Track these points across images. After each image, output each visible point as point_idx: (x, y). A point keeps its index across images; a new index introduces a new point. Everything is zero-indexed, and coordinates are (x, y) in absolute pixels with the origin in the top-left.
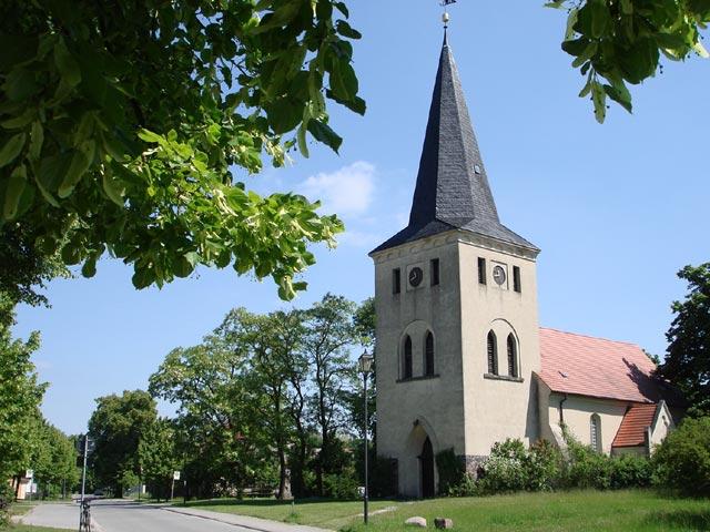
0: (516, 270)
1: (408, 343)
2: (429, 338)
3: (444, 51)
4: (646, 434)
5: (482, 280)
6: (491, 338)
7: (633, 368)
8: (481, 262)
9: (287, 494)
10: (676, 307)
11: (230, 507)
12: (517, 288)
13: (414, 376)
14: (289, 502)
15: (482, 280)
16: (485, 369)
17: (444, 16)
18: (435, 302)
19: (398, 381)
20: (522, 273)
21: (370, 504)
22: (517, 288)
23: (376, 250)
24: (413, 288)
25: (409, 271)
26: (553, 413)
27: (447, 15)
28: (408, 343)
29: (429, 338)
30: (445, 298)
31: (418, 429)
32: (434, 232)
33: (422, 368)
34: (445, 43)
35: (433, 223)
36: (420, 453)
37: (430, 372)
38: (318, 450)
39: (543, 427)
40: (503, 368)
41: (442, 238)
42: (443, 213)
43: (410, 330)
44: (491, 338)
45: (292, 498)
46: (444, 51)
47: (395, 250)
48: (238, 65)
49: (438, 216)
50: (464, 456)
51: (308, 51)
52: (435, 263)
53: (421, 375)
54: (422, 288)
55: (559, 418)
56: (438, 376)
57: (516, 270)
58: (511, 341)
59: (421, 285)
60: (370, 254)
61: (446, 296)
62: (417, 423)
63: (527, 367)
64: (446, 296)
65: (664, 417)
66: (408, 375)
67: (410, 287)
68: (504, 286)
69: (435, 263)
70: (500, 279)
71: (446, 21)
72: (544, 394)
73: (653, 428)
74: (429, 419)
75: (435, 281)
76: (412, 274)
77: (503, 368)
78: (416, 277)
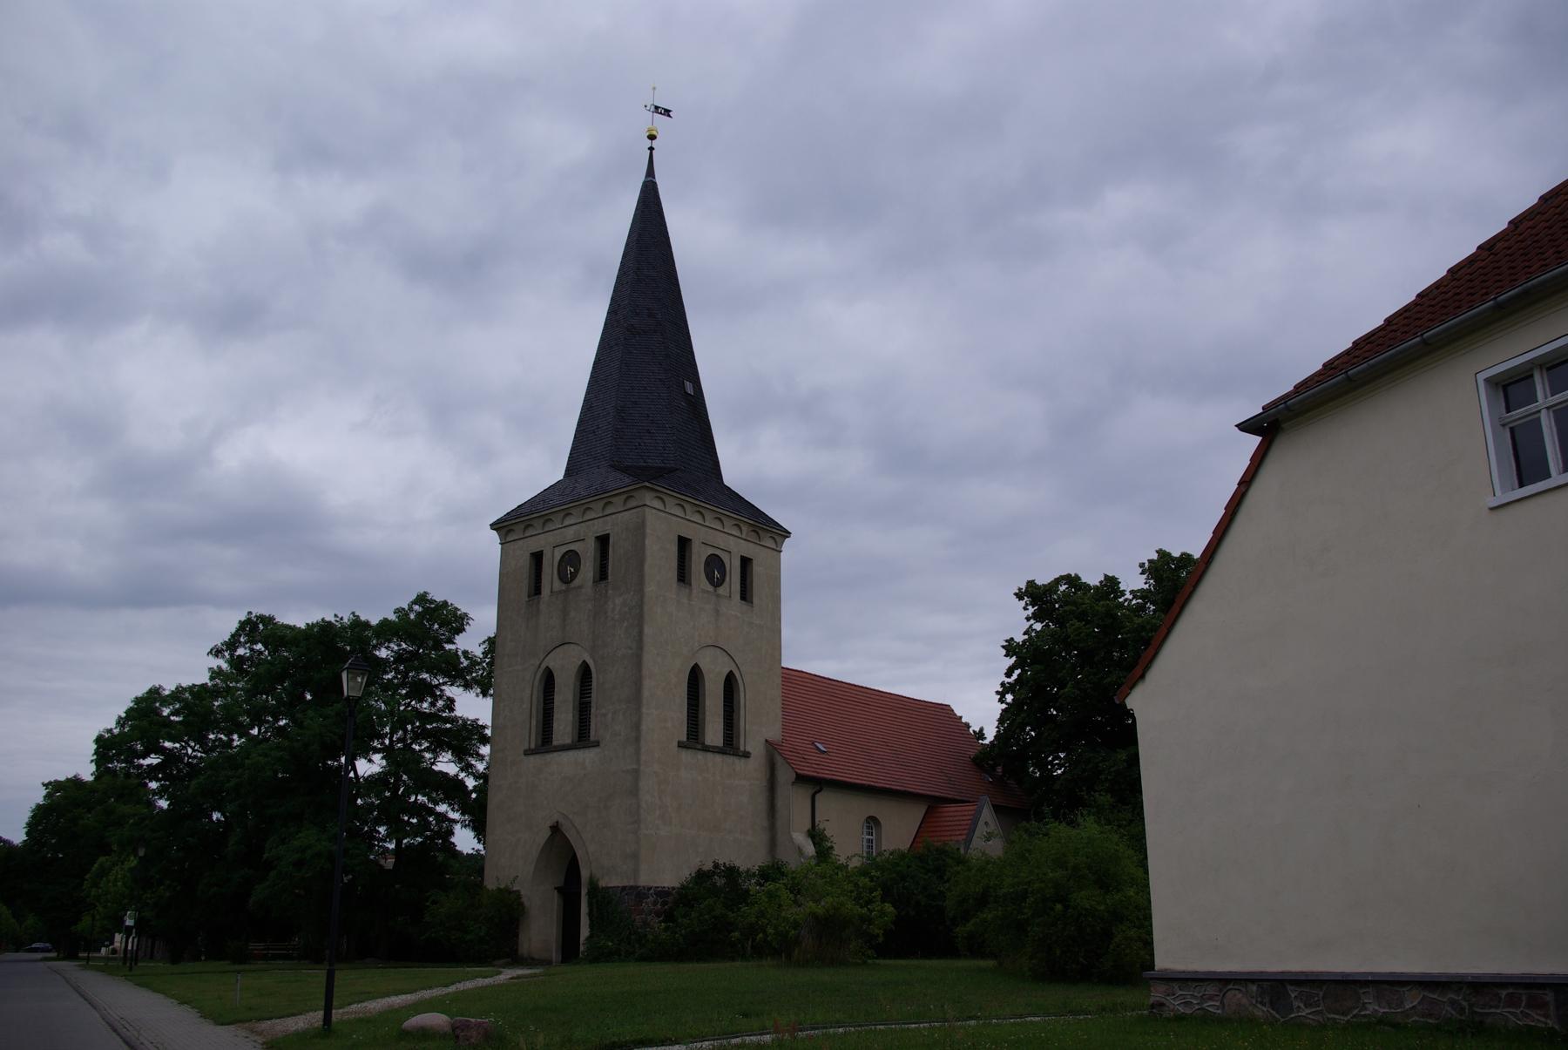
0: (746, 562)
2: (585, 674)
5: (683, 576)
6: (695, 677)
8: (684, 544)
19: (528, 752)
22: (746, 594)
24: (564, 587)
25: (558, 557)
29: (585, 674)
33: (569, 729)
36: (560, 883)
37: (583, 738)
44: (695, 677)
52: (603, 541)
53: (568, 741)
54: (580, 587)
56: (597, 744)
57: (746, 562)
58: (730, 683)
59: (576, 582)
60: (496, 526)
64: (618, 601)
67: (558, 585)
69: (603, 541)
75: (602, 574)
77: (714, 732)
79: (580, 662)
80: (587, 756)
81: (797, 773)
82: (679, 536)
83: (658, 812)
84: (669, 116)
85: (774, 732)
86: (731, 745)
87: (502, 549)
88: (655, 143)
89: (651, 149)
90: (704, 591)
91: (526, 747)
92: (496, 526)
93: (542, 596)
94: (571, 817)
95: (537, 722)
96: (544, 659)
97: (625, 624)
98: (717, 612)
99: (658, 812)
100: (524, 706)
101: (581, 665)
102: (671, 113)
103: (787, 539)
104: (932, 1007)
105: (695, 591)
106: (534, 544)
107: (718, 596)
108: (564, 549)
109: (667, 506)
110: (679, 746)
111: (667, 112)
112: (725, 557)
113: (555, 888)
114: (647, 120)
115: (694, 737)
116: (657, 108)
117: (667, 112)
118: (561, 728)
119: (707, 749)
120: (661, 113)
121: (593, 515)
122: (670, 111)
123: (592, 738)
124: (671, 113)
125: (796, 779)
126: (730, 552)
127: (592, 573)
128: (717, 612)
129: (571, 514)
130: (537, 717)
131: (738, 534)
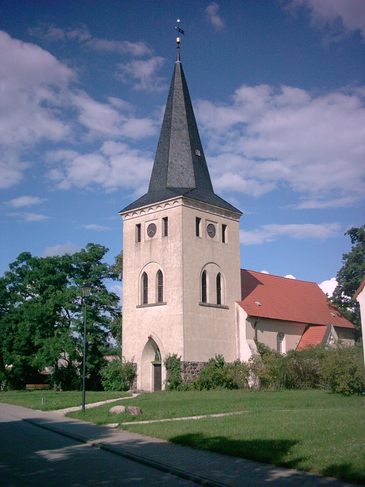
1: (145, 275)
2: (160, 273)
10: (345, 256)
13: (149, 303)
24: (150, 239)
25: (147, 226)
28: (145, 275)
29: (160, 273)
33: (154, 297)
40: (211, 298)
48: (98, 361)
51: (277, 333)
53: (154, 302)
55: (254, 335)
56: (166, 304)
59: (155, 237)
61: (172, 245)
64: (172, 245)
67: (147, 238)
74: (159, 335)
77: (211, 298)
78: (152, 230)
83: (191, 332)
93: (141, 242)
94: (156, 333)
99: (191, 332)
100: (136, 288)
111: (183, 32)
118: (151, 297)
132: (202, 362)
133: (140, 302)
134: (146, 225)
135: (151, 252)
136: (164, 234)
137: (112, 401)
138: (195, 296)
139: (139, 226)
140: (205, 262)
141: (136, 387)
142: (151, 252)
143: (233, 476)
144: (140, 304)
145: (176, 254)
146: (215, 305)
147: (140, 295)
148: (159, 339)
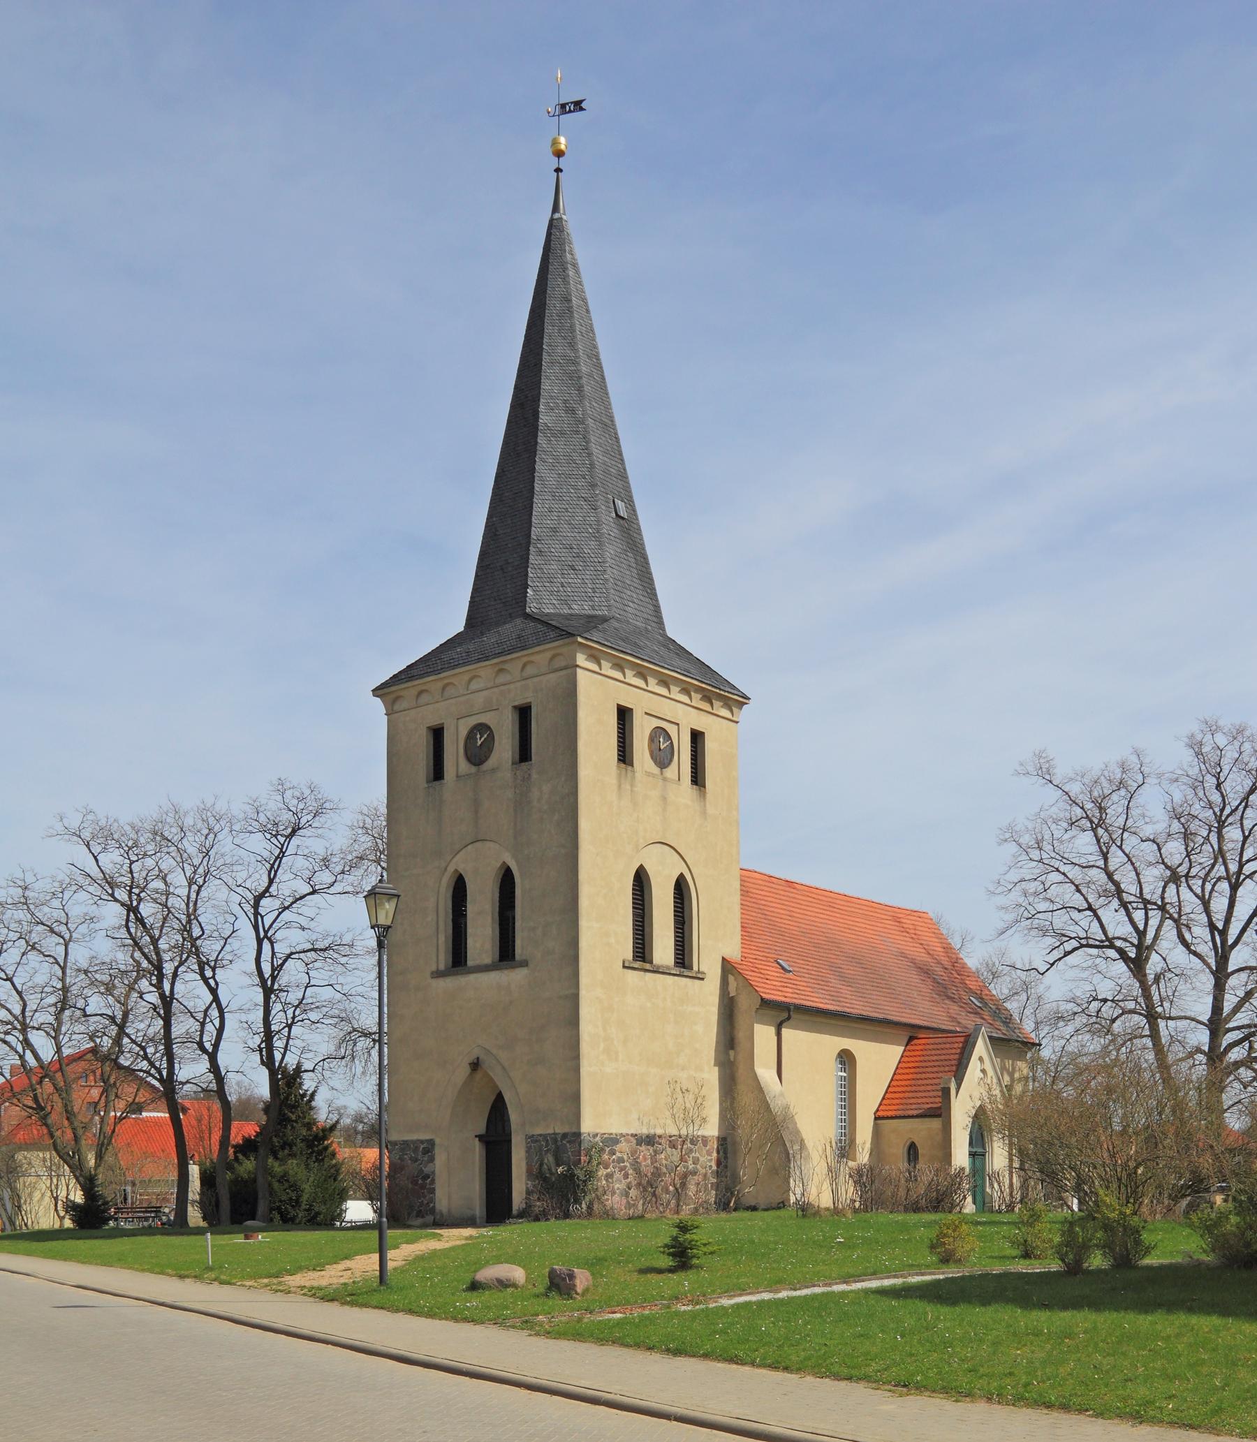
0: (697, 737)
2: (507, 881)
3: (555, 231)
4: (946, 1092)
5: (625, 755)
6: (641, 881)
7: (913, 961)
8: (624, 714)
9: (194, 1216)
11: (807, 1018)
12: (698, 778)
13: (470, 963)
14: (199, 1231)
15: (625, 755)
16: (626, 949)
17: (555, 142)
18: (521, 804)
19: (438, 974)
20: (710, 745)
21: (391, 1233)
22: (698, 778)
23: (396, 679)
24: (473, 769)
25: (464, 732)
26: (763, 1035)
27: (562, 140)
29: (507, 881)
30: (543, 791)
31: (478, 1075)
32: (521, 645)
33: (488, 946)
34: (556, 208)
35: (518, 621)
36: (482, 1129)
37: (506, 953)
38: (280, 1076)
39: (741, 1072)
41: (541, 656)
42: (541, 600)
43: (462, 863)
44: (641, 881)
45: (203, 1224)
46: (555, 231)
47: (432, 683)
49: (532, 607)
50: (578, 1134)
52: (524, 713)
53: (487, 960)
54: (493, 770)
56: (524, 964)
57: (697, 737)
58: (681, 889)
59: (492, 762)
60: (379, 691)
62: (475, 1065)
63: (708, 958)
64: (546, 788)
65: (981, 1059)
66: (458, 958)
67: (464, 766)
68: (671, 772)
69: (524, 713)
70: (663, 758)
71: (559, 154)
72: (746, 1004)
73: (959, 1075)
75: (524, 754)
76: (470, 736)
77: (664, 950)
78: (478, 753)
79: (499, 865)
80: (514, 978)
81: (762, 999)
82: (618, 705)
83: (602, 1045)
84: (582, 109)
85: (732, 948)
86: (683, 957)
87: (389, 721)
88: (563, 163)
89: (558, 170)
90: (649, 774)
91: (434, 968)
92: (379, 691)
93: (445, 781)
94: (494, 1052)
95: (446, 937)
96: (450, 861)
97: (556, 817)
98: (664, 799)
99: (602, 1045)
100: (429, 919)
101: (500, 868)
102: (583, 105)
103: (745, 706)
104: (1019, 1352)
105: (637, 775)
106: (432, 714)
107: (665, 779)
108: (473, 721)
109: (603, 667)
110: (624, 967)
111: (578, 105)
112: (672, 730)
113: (476, 1136)
114: (554, 162)
115: (642, 950)
116: (563, 106)
117: (578, 105)
118: (478, 945)
119: (656, 971)
120: (570, 111)
121: (508, 678)
122: (581, 102)
123: (517, 957)
124: (583, 105)
125: (760, 1006)
126: (678, 724)
127: (510, 753)
128: (664, 799)
129: (479, 676)
130: (446, 931)
131: (688, 701)
132: (632, 1135)
133: (443, 959)
134: (461, 728)
135: (476, 812)
136: (517, 757)
137: (1219, 945)
138: (612, 940)
139: (437, 734)
140: (641, 841)
141: (434, 1207)
142: (476, 812)
143: (684, 1308)
144: (442, 967)
145: (556, 817)
146: (668, 967)
147: (442, 938)
148: (504, 1068)
